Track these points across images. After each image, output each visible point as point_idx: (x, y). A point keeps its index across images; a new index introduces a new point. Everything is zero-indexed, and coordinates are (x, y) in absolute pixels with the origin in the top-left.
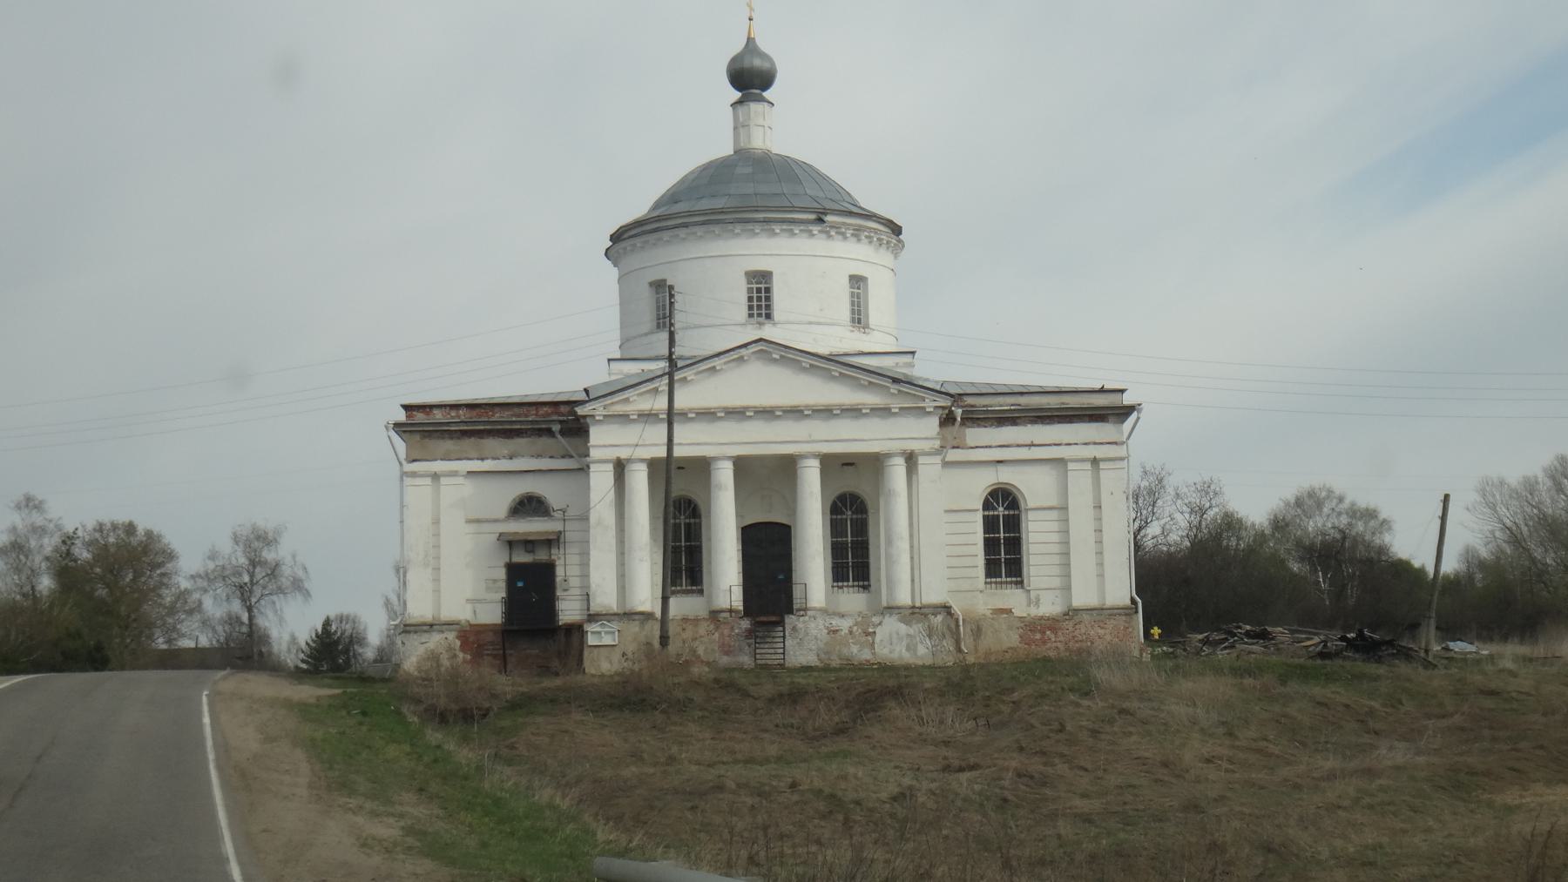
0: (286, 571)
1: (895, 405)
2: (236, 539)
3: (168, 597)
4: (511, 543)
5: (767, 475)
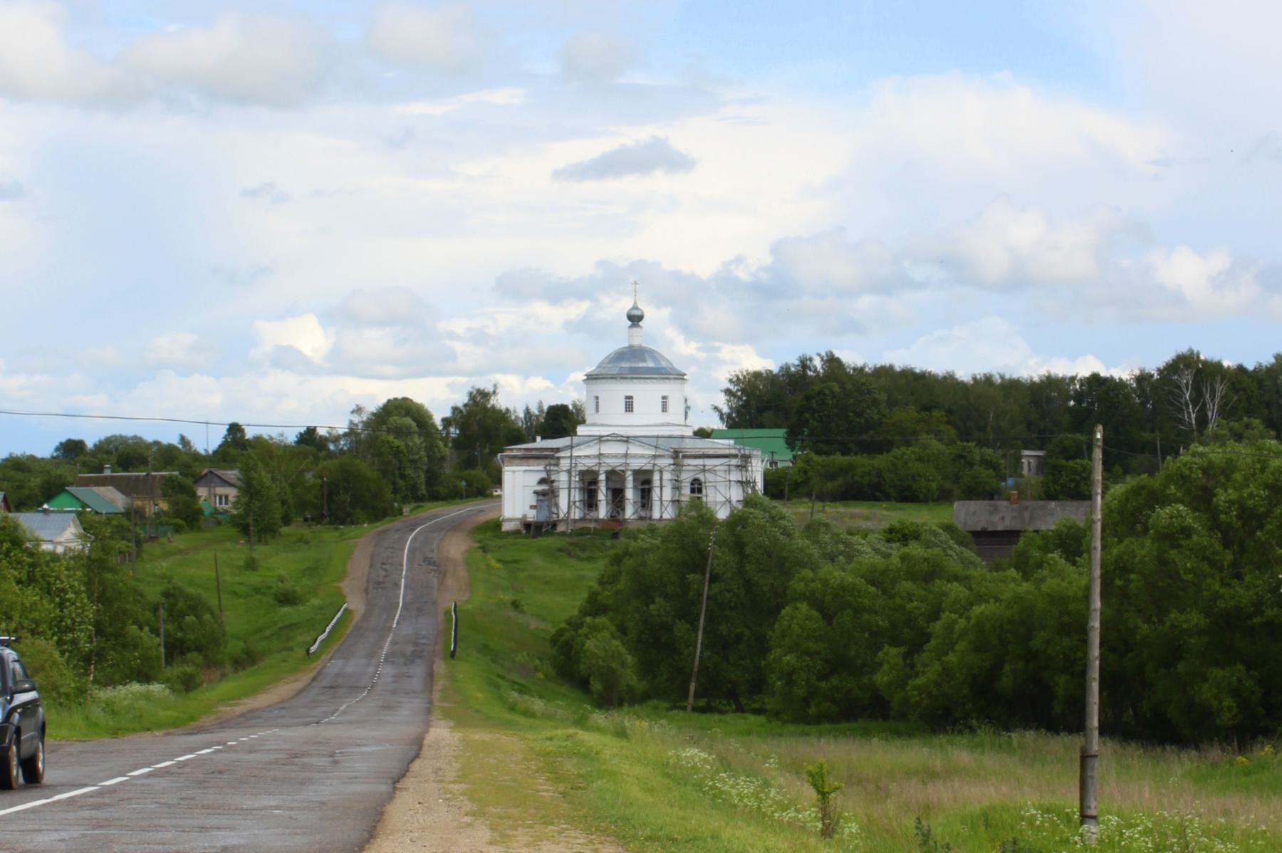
5: (615, 477)
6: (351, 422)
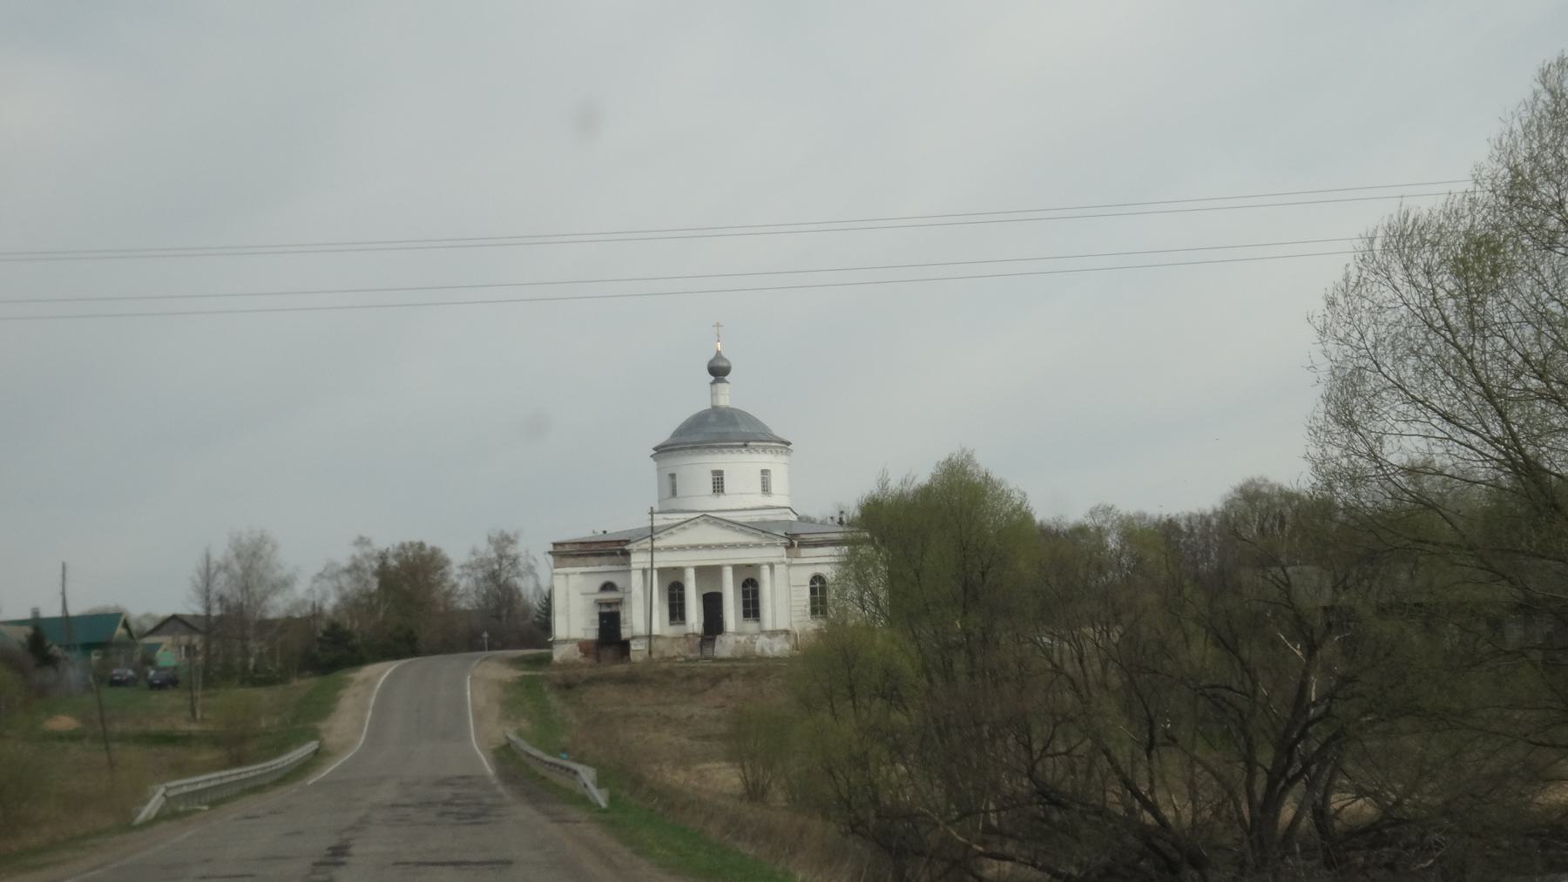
0: (522, 560)
1: (764, 542)
2: (490, 540)
3: (447, 586)
4: (600, 604)
5: (708, 573)
6: (354, 557)
